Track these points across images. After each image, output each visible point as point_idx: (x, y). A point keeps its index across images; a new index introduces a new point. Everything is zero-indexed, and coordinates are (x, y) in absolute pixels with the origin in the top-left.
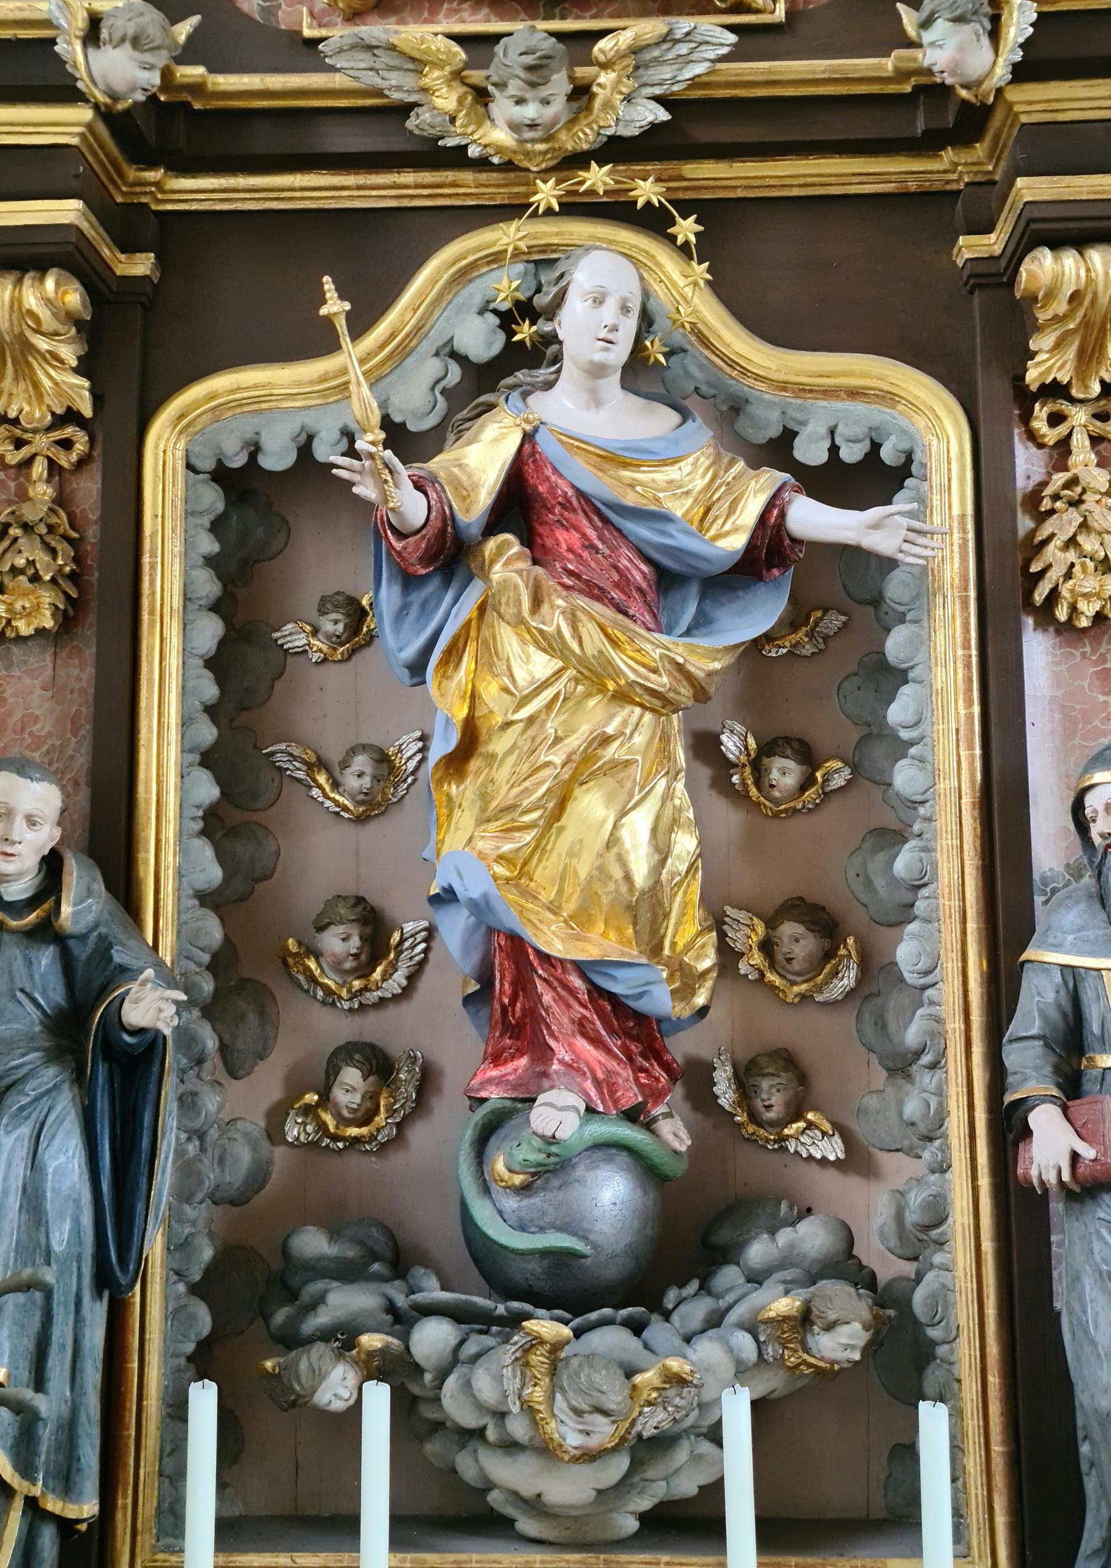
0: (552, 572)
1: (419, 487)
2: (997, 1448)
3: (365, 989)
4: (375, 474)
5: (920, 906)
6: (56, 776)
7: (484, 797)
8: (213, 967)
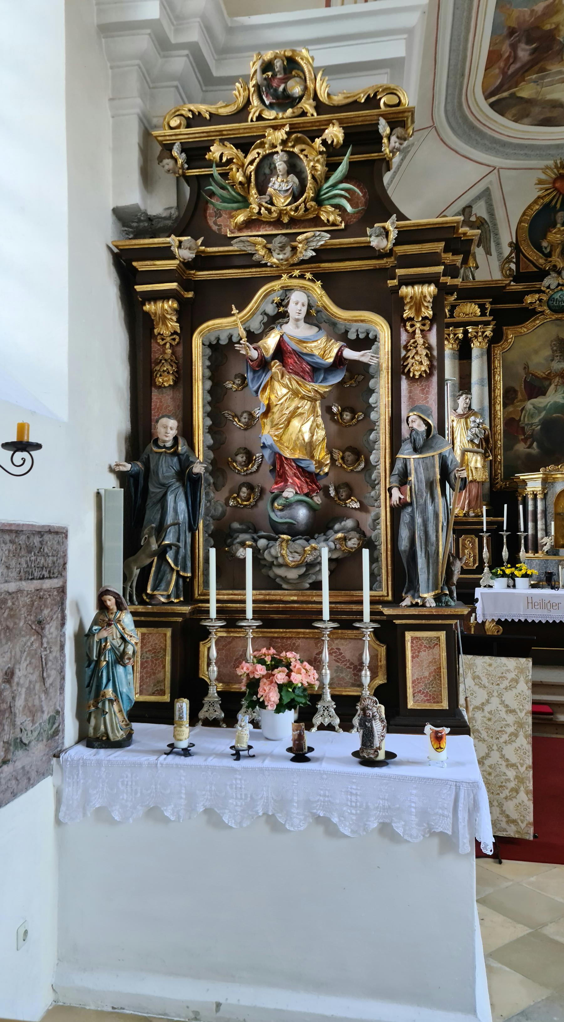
0: (287, 369)
1: (255, 349)
2: (390, 568)
3: (247, 470)
4: (245, 348)
5: (376, 447)
6: (176, 418)
7: (272, 421)
8: (211, 464)
